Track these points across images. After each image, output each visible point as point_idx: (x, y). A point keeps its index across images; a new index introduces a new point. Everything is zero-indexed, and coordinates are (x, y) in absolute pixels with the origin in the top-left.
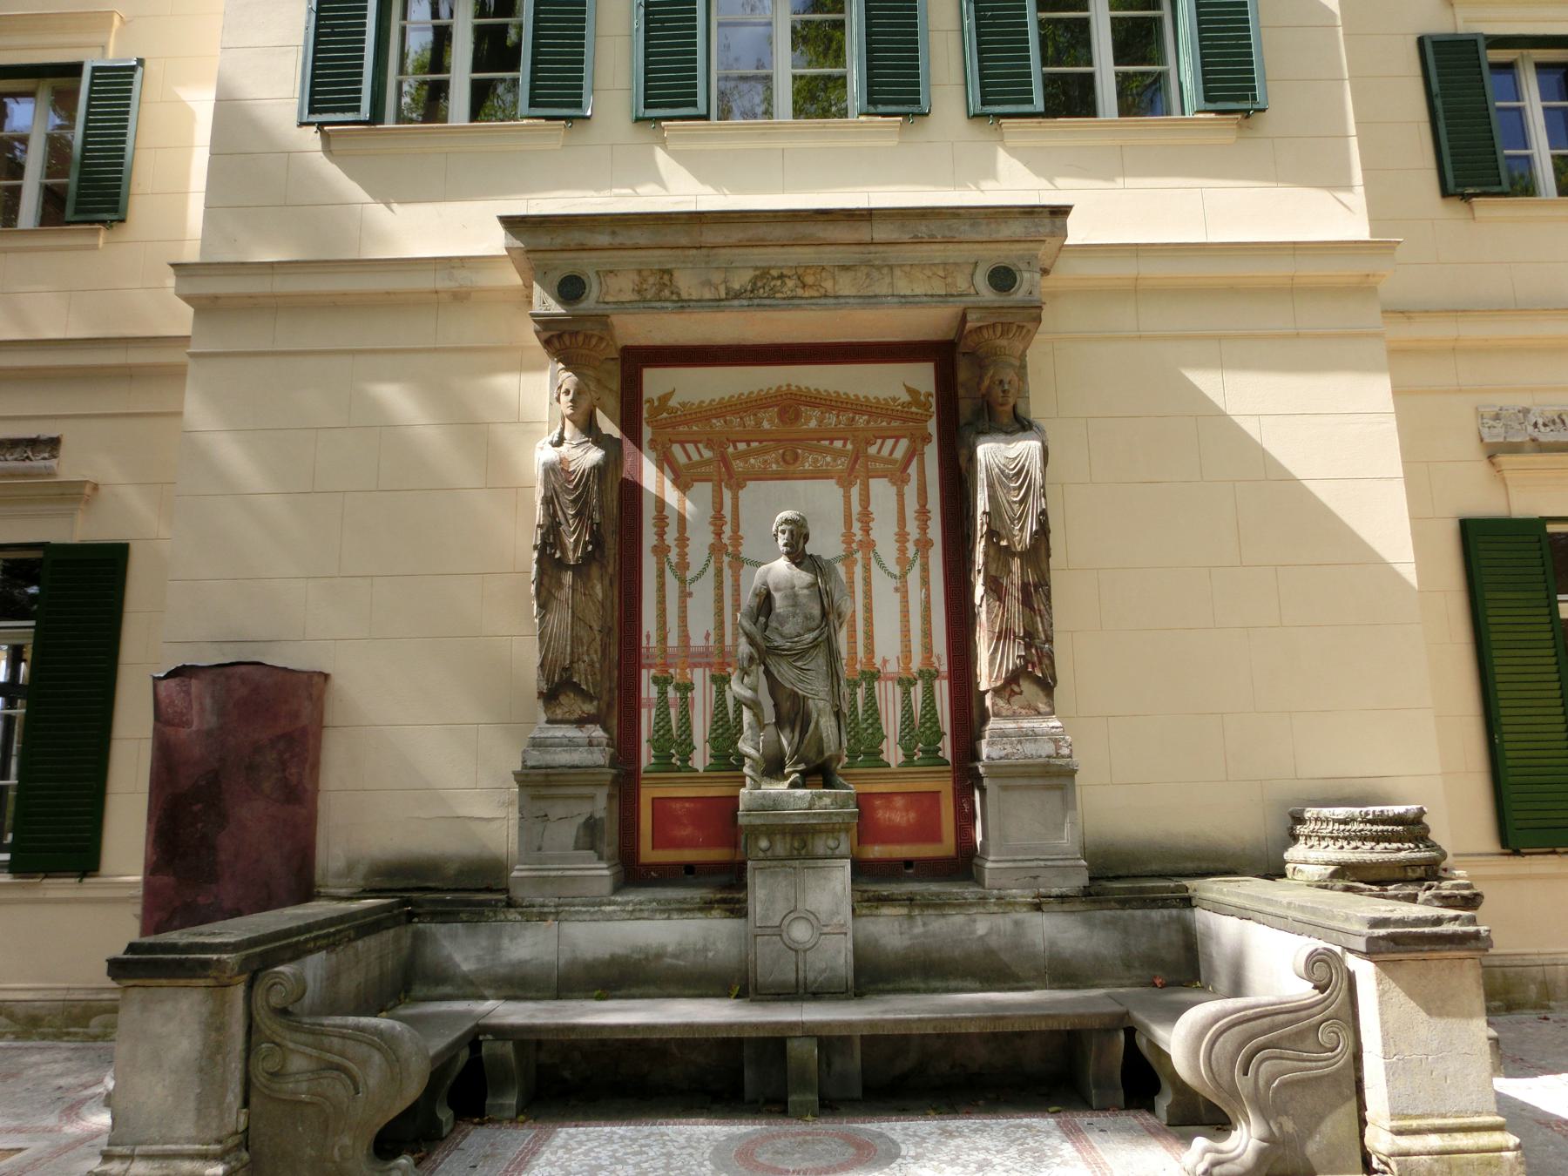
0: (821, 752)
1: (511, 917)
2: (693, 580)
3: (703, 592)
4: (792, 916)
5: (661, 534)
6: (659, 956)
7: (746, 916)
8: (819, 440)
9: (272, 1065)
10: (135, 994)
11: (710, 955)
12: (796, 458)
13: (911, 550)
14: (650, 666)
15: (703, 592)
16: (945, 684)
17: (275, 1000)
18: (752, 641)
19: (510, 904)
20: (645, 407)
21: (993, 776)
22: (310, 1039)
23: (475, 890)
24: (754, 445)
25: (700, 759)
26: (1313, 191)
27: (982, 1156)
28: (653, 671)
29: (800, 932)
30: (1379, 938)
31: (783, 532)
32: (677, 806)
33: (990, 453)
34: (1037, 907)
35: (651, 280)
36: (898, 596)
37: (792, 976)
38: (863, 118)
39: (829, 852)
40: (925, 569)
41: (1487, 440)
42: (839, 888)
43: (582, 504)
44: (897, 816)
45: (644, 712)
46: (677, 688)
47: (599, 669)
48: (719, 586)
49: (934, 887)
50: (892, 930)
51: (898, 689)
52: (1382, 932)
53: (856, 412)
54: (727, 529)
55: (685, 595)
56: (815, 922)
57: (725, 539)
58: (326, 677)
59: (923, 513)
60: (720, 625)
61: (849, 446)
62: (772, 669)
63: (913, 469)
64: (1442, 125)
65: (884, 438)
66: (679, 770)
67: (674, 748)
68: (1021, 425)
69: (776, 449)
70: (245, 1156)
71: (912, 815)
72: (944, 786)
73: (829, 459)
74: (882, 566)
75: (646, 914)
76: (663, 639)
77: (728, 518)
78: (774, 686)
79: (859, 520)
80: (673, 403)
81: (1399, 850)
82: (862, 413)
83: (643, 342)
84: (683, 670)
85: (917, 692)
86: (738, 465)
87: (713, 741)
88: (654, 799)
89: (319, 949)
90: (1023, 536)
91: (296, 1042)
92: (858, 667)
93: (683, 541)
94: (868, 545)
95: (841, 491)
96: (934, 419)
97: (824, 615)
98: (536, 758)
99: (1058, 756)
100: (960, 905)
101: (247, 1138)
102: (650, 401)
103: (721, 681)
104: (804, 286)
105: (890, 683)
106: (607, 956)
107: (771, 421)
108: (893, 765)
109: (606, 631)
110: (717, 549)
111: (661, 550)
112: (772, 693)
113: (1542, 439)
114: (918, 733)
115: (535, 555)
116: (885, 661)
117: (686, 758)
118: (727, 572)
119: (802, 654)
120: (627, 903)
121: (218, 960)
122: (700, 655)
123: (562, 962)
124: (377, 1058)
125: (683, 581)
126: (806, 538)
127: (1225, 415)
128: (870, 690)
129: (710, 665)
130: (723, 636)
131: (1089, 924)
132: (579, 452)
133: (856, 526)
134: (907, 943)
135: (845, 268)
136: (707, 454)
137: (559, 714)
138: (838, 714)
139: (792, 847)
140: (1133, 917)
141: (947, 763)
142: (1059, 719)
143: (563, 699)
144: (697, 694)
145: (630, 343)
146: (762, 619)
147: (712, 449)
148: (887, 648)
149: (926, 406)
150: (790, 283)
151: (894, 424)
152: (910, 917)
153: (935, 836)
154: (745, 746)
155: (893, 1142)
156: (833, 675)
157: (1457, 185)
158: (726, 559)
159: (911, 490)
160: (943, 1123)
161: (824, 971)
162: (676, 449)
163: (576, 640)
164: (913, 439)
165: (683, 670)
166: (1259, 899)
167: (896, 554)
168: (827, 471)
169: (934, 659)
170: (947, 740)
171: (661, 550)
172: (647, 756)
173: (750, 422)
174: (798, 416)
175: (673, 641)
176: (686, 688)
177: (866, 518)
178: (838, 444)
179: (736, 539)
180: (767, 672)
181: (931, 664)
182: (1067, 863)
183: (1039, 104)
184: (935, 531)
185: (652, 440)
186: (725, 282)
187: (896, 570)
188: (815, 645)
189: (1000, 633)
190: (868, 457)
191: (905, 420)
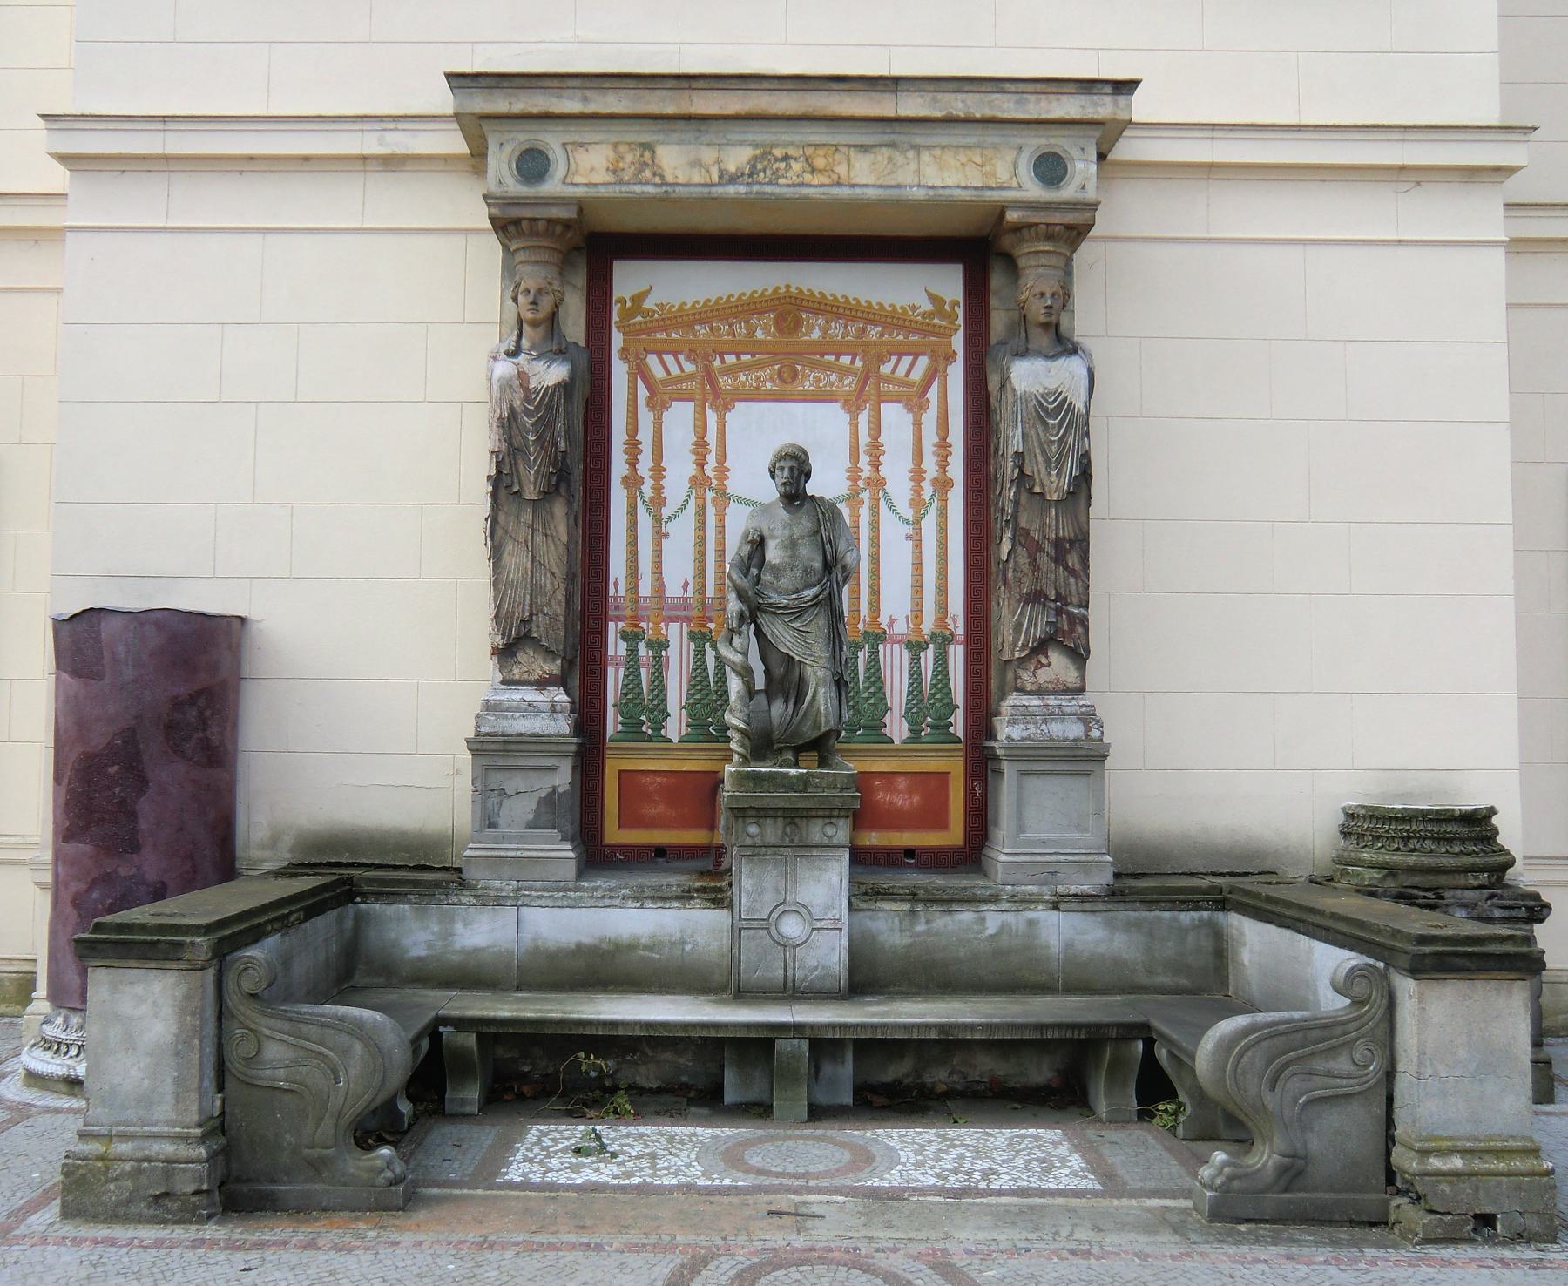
0: (817, 725)
1: (464, 900)
2: (670, 519)
3: (681, 534)
4: (782, 908)
5: (633, 463)
6: (632, 946)
7: (730, 907)
8: (822, 355)
9: (248, 1049)
12: (795, 375)
13: (928, 490)
14: (618, 619)
15: (681, 534)
16: (961, 649)
17: (247, 986)
18: (741, 596)
19: (463, 884)
20: (616, 308)
21: (1013, 758)
22: (286, 1026)
23: (419, 871)
24: (745, 358)
25: (675, 728)
27: (985, 1166)
28: (621, 625)
29: (792, 927)
31: (782, 469)
33: (1028, 376)
34: (1055, 906)
35: (629, 158)
39: (826, 841)
40: (943, 515)
43: (544, 425)
44: (901, 799)
45: (611, 672)
46: (649, 645)
47: (565, 622)
48: (701, 526)
49: (939, 881)
50: (891, 927)
51: (906, 655)
52: (1427, 949)
53: (868, 321)
54: (711, 459)
55: (660, 536)
57: (709, 472)
58: (242, 620)
59: (943, 447)
60: (701, 573)
61: (858, 364)
62: (765, 630)
63: (933, 394)
65: (900, 355)
67: (645, 713)
68: (1063, 345)
69: (771, 364)
70: (222, 1141)
71: (916, 798)
72: (955, 767)
73: (833, 378)
75: (616, 902)
77: (713, 445)
78: (766, 647)
80: (649, 304)
82: (875, 323)
83: (619, 229)
85: (928, 657)
86: (726, 382)
87: (690, 707)
89: (276, 931)
92: (861, 626)
93: (658, 471)
94: (877, 483)
95: (847, 417)
96: (960, 333)
97: (828, 566)
98: (494, 724)
99: (1088, 738)
100: (969, 901)
101: (222, 1124)
102: (622, 301)
103: (700, 638)
104: (813, 170)
105: (896, 646)
106: (573, 946)
107: (765, 329)
108: (897, 742)
109: (570, 579)
111: (632, 482)
112: (763, 658)
114: (927, 706)
117: (659, 726)
118: (710, 511)
119: (799, 613)
120: (595, 889)
121: (192, 943)
122: (676, 607)
123: (522, 950)
124: (358, 1047)
125: (657, 519)
126: (808, 476)
128: (874, 653)
129: (688, 619)
131: (1110, 925)
132: (540, 366)
133: (864, 461)
134: (907, 941)
136: (689, 367)
137: (517, 673)
138: (839, 684)
139: (784, 833)
143: (521, 656)
144: (673, 653)
145: (599, 228)
146: (754, 571)
147: (694, 361)
148: (895, 607)
149: (952, 317)
150: (796, 166)
152: (912, 913)
153: (942, 824)
154: (733, 719)
155: (891, 1149)
158: (709, 495)
159: (930, 418)
160: (942, 1132)
161: (816, 969)
162: (652, 360)
163: (535, 589)
164: (934, 358)
167: (909, 495)
168: (831, 393)
169: (949, 620)
170: (960, 713)
171: (632, 482)
172: (613, 723)
173: (741, 330)
174: (798, 323)
175: (645, 589)
176: (660, 645)
177: (876, 449)
178: (845, 360)
179: (722, 471)
180: (759, 633)
181: (946, 626)
182: (1090, 858)
184: (957, 469)
185: (624, 350)
187: (909, 514)
188: (815, 602)
190: (881, 378)
191: (925, 333)
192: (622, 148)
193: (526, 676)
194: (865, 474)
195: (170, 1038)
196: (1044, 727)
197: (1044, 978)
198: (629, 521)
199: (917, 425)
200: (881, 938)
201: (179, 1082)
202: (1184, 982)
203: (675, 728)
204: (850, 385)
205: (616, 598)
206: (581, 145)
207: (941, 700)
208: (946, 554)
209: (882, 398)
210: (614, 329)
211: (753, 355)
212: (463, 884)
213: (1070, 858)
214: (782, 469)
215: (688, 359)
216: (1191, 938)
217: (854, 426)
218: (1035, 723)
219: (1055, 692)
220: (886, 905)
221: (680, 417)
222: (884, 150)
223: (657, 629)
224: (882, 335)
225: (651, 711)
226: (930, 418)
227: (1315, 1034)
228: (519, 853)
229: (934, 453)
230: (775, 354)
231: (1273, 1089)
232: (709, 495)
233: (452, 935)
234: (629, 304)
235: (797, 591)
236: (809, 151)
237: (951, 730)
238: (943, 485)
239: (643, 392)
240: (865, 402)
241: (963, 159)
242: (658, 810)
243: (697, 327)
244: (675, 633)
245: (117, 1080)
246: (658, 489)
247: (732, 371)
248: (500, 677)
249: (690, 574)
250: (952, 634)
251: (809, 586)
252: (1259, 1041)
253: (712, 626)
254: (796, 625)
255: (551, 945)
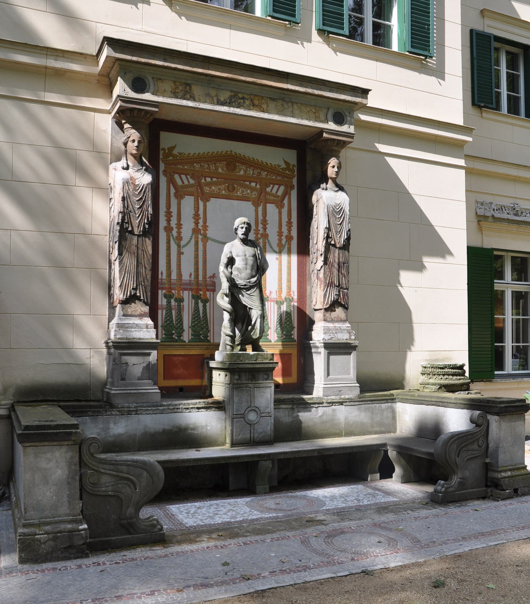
2: (184, 246)
3: (189, 252)
4: (249, 409)
5: (169, 221)
8: (245, 181)
10: (30, 450)
11: (208, 428)
14: (163, 289)
19: (112, 406)
20: (161, 152)
24: (214, 179)
25: (186, 336)
26: (441, 95)
28: (164, 291)
29: (252, 417)
30: (503, 407)
32: (176, 358)
36: (277, 261)
37: (248, 436)
38: (270, 18)
41: (478, 214)
42: (269, 396)
45: (160, 312)
46: (176, 300)
48: (197, 250)
51: (276, 306)
53: (262, 169)
54: (201, 221)
56: (259, 412)
59: (289, 223)
61: (258, 186)
63: (286, 201)
64: (475, 71)
65: (274, 184)
66: (176, 341)
73: (249, 191)
74: (271, 247)
76: (169, 274)
77: (201, 216)
79: (261, 223)
80: (175, 152)
81: (460, 379)
82: (264, 170)
83: (169, 118)
84: (179, 291)
86: (207, 189)
87: (193, 327)
88: (164, 355)
90: (340, 240)
91: (104, 469)
93: (179, 226)
95: (254, 208)
96: (296, 178)
102: (164, 149)
105: (272, 303)
106: (161, 430)
110: (196, 231)
111: (168, 229)
113: (496, 216)
115: (118, 228)
116: (271, 293)
117: (180, 335)
118: (200, 244)
122: (186, 284)
124: (145, 474)
125: (179, 246)
127: (409, 193)
129: (191, 290)
130: (198, 275)
133: (260, 226)
134: (291, 420)
135: (273, 99)
136: (192, 181)
140: (375, 406)
141: (295, 341)
142: (350, 323)
144: (185, 304)
149: (292, 171)
151: (278, 178)
156: (262, 300)
157: (478, 101)
158: (200, 237)
159: (285, 211)
161: (262, 433)
162: (176, 177)
164: (286, 187)
165: (179, 291)
166: (48, 421)
167: (277, 242)
168: (248, 197)
169: (292, 293)
171: (168, 229)
173: (213, 167)
174: (235, 167)
175: (174, 276)
176: (180, 300)
178: (253, 184)
179: (205, 227)
181: (290, 295)
183: (346, 31)
186: (217, 96)
189: (329, 283)
190: (267, 193)
191: (284, 177)
192: (177, 84)
193: (134, 313)
194: (261, 232)
195: (65, 476)
196: (336, 335)
197: (338, 431)
198: (167, 246)
199: (280, 213)
200: (281, 419)
201: (69, 496)
202: (383, 429)
203: (186, 336)
204: (255, 195)
205: (162, 279)
206: (160, 79)
207: (289, 325)
208: (290, 266)
209: (267, 202)
210: (161, 162)
211: (217, 179)
212: (112, 406)
213: (345, 385)
214: (242, 228)
215: (191, 178)
216: (385, 413)
217: (257, 212)
218: (333, 333)
219: (337, 321)
220: (283, 406)
221: (188, 202)
222: (280, 101)
223: (179, 293)
224: (267, 175)
225: (177, 329)
226: (285, 211)
227: (470, 437)
228: (136, 391)
229: (286, 225)
230: (226, 179)
231: (458, 457)
232: (200, 237)
233: (109, 429)
234: (167, 151)
235: (249, 279)
236: (252, 97)
237: (292, 337)
238: (289, 238)
239: (173, 191)
240: (261, 202)
241: (309, 110)
242: (180, 371)
243: (195, 165)
244: (186, 295)
245: (40, 498)
246: (179, 233)
247: (209, 185)
248: (122, 314)
249: (192, 270)
250: (293, 298)
251: (253, 277)
252: (455, 440)
253: (201, 293)
254: (248, 292)
255: (152, 431)
